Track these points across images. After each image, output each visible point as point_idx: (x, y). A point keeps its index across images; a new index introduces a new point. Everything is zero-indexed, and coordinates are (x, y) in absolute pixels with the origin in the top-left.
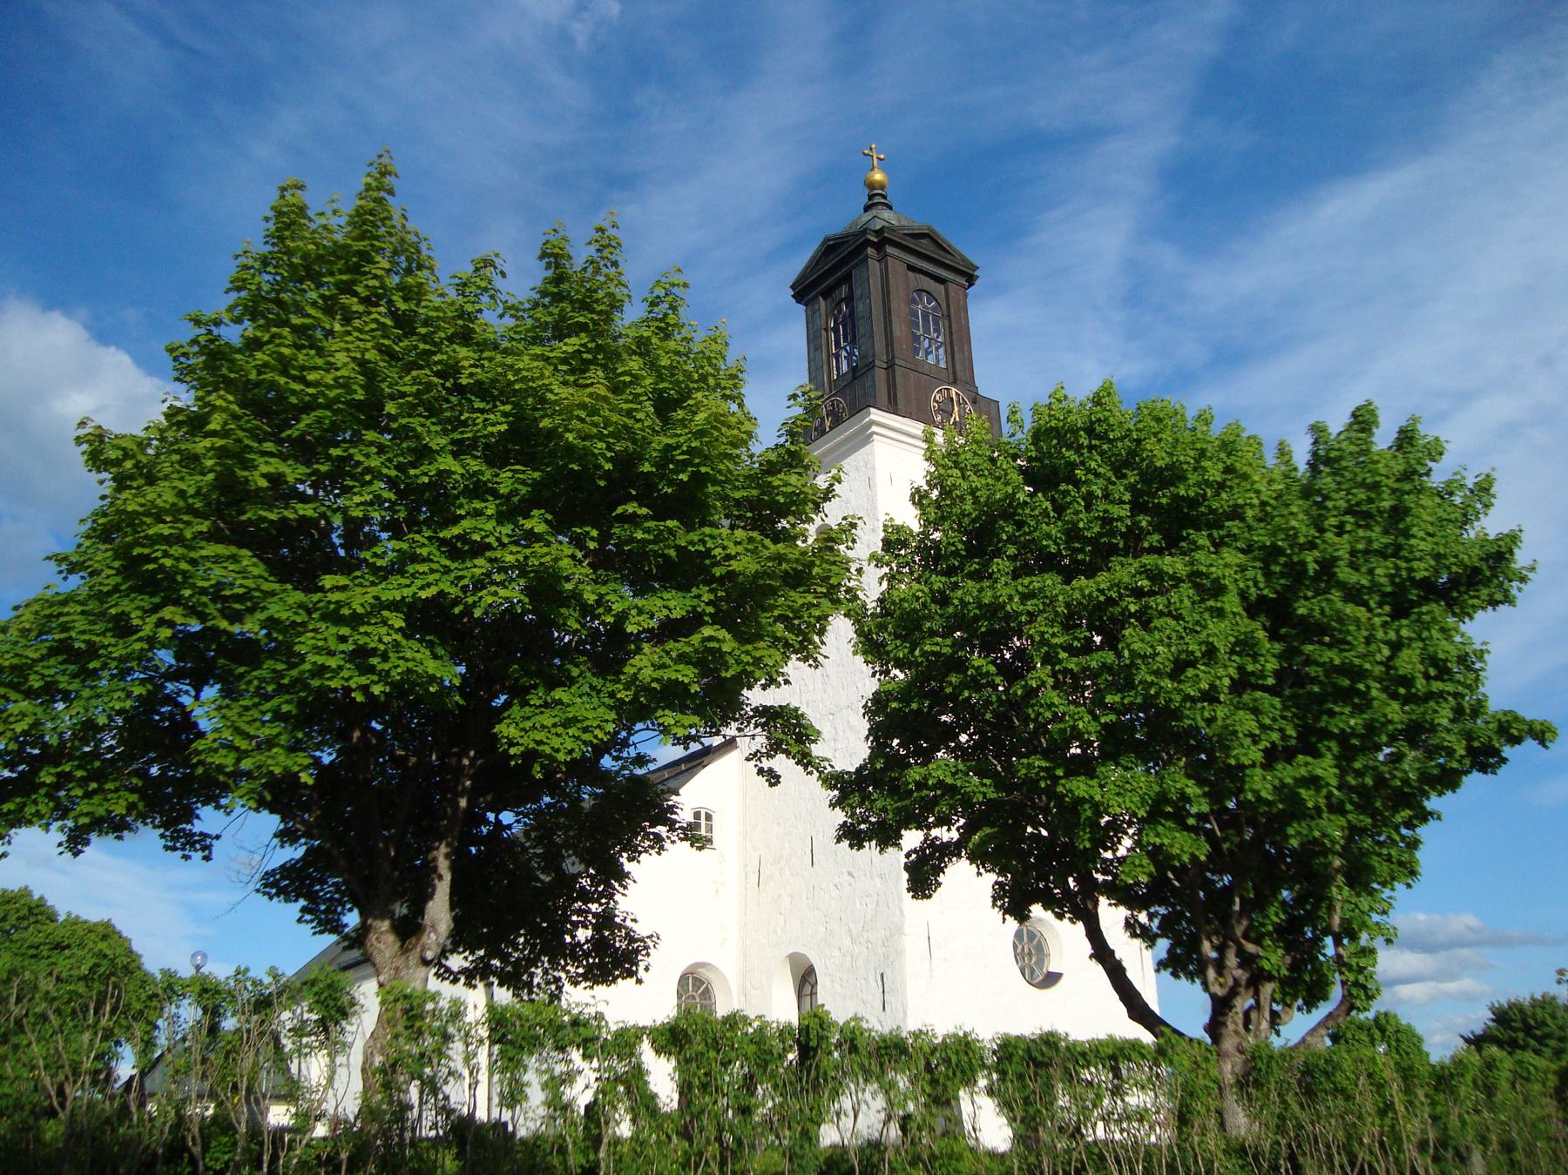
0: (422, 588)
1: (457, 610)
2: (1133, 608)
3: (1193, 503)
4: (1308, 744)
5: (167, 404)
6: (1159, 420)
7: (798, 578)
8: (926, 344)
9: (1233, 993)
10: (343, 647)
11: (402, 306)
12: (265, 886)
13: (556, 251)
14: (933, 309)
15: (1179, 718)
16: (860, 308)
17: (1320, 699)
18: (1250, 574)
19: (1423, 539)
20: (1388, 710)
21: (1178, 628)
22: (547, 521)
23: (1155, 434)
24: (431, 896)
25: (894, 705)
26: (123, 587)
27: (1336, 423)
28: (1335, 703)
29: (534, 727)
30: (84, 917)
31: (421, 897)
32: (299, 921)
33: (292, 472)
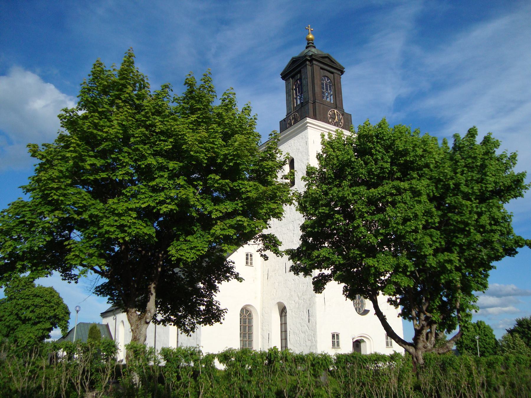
0: (143, 204)
1: (154, 211)
2: (390, 200)
3: (412, 162)
4: (448, 249)
5: (59, 134)
6: (401, 133)
7: (273, 198)
8: (327, 94)
9: (422, 328)
10: (116, 224)
11: (137, 102)
12: (96, 291)
13: (190, 82)
14: (329, 82)
15: (405, 238)
16: (304, 82)
17: (454, 231)
18: (431, 188)
19: (491, 177)
20: (476, 237)
21: (405, 207)
22: (185, 180)
23: (400, 138)
24: (148, 301)
25: (309, 229)
26: (43, 202)
27: (463, 134)
28: (458, 233)
29: (180, 249)
30: (44, 286)
31: (146, 300)
32: (108, 303)
33: (99, 163)
